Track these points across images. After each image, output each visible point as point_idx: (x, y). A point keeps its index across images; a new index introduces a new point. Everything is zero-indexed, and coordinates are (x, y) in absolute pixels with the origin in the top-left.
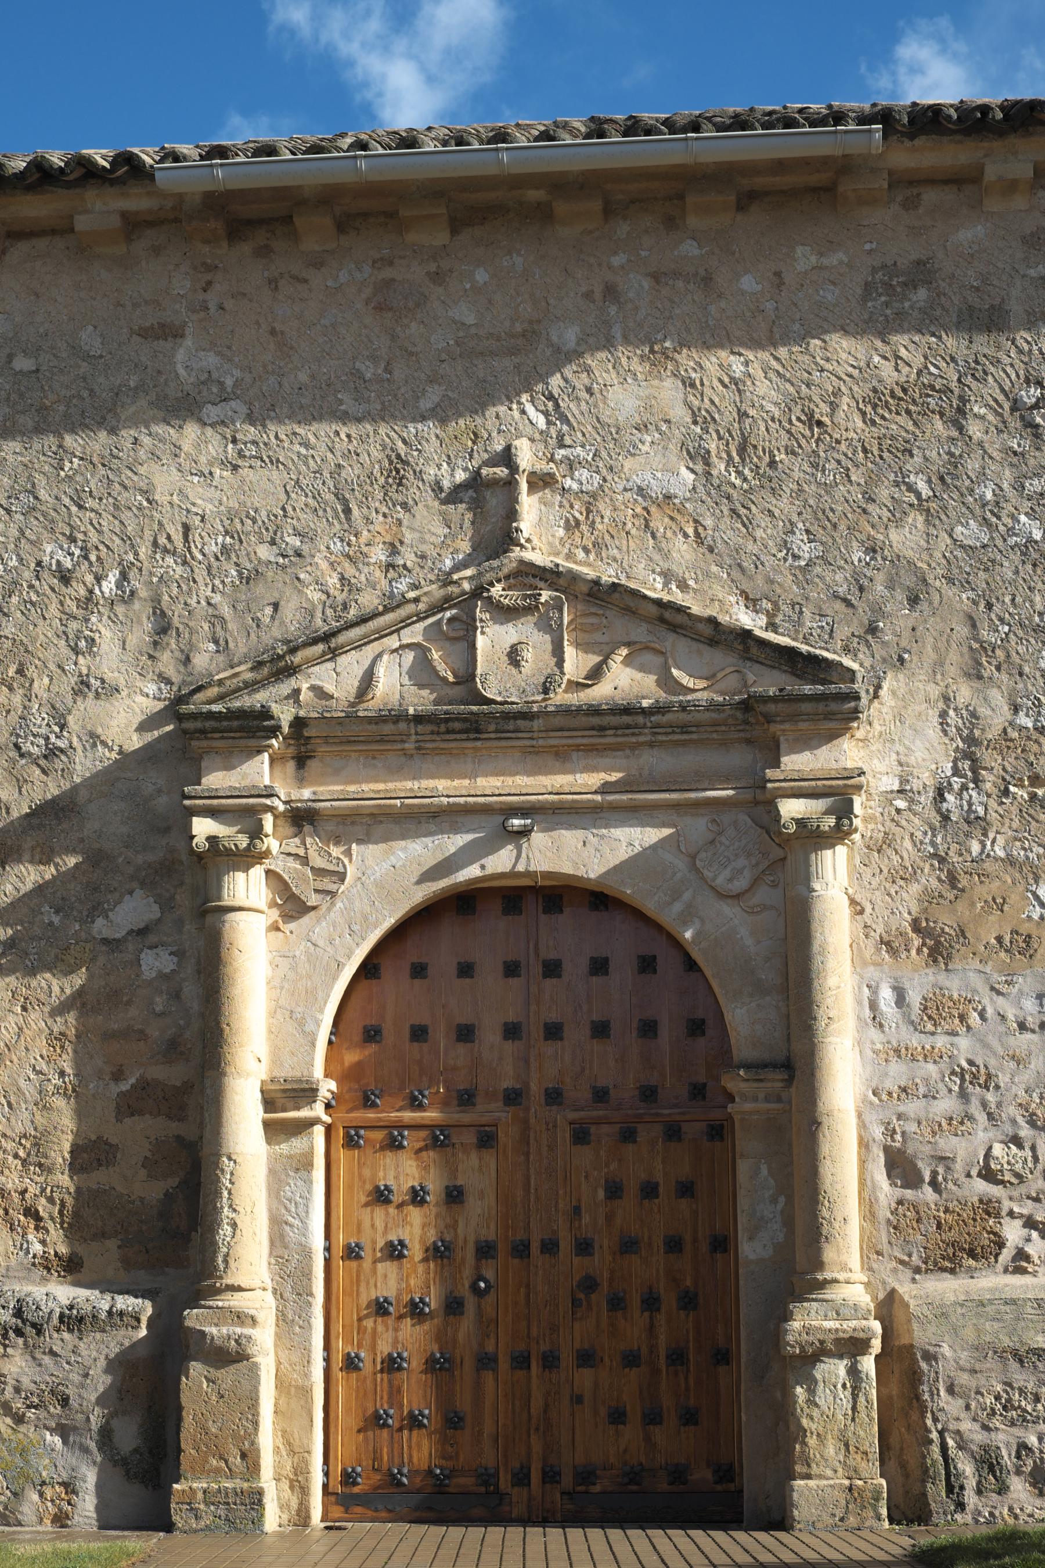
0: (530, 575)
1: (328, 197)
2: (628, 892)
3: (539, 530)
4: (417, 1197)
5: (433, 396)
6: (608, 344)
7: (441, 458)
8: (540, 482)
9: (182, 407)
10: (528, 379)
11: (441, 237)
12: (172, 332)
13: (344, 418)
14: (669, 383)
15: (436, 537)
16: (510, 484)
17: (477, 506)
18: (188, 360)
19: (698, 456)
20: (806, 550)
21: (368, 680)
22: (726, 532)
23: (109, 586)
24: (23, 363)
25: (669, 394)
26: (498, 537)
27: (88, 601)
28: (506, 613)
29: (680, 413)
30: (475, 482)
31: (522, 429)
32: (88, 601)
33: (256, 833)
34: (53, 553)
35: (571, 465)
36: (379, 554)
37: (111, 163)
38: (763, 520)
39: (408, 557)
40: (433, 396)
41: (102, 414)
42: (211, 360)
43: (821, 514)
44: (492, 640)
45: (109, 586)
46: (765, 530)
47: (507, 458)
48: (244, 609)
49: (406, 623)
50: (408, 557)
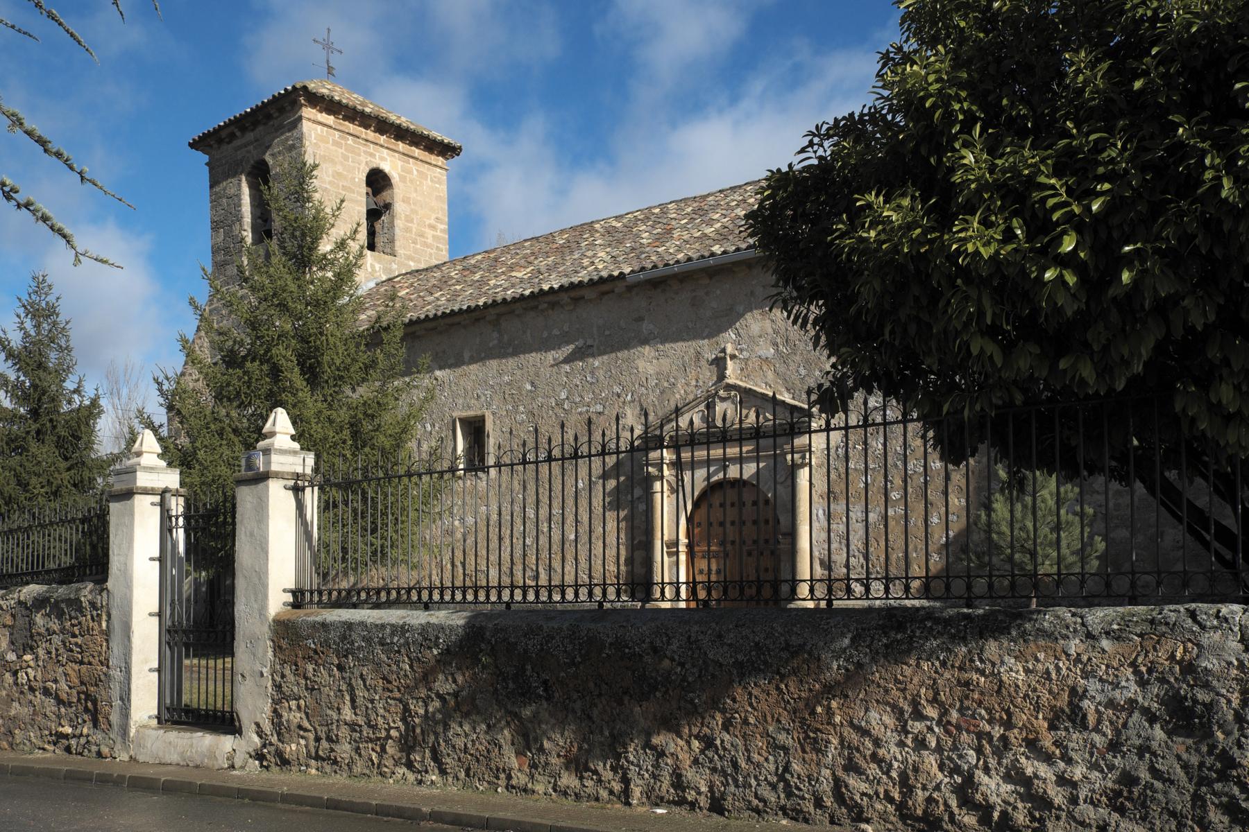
0: (729, 387)
1: (675, 276)
2: (261, 485)
3: (732, 373)
4: (1019, 626)
5: (707, 331)
6: (751, 310)
7: (708, 350)
8: (733, 357)
9: (644, 342)
10: (730, 324)
11: (707, 281)
12: (640, 319)
13: (684, 340)
14: (768, 321)
15: (708, 376)
16: (725, 358)
17: (718, 366)
18: (646, 327)
19: (775, 344)
20: (803, 372)
21: (691, 422)
22: (781, 368)
23: (629, 398)
24: (607, 333)
25: (768, 324)
26: (721, 376)
27: (624, 402)
28: (723, 400)
29: (770, 331)
30: (717, 359)
31: (729, 341)
32: (624, 402)
33: (661, 470)
34: (617, 389)
35: (741, 350)
36: (694, 383)
37: (1025, 138)
38: (792, 364)
39: (701, 383)
40: (707, 331)
41: (626, 346)
42: (651, 326)
43: (807, 361)
44: (720, 408)
45: (629, 398)
46: (793, 367)
47: (724, 351)
48: (661, 402)
49: (699, 404)
50: (701, 383)
